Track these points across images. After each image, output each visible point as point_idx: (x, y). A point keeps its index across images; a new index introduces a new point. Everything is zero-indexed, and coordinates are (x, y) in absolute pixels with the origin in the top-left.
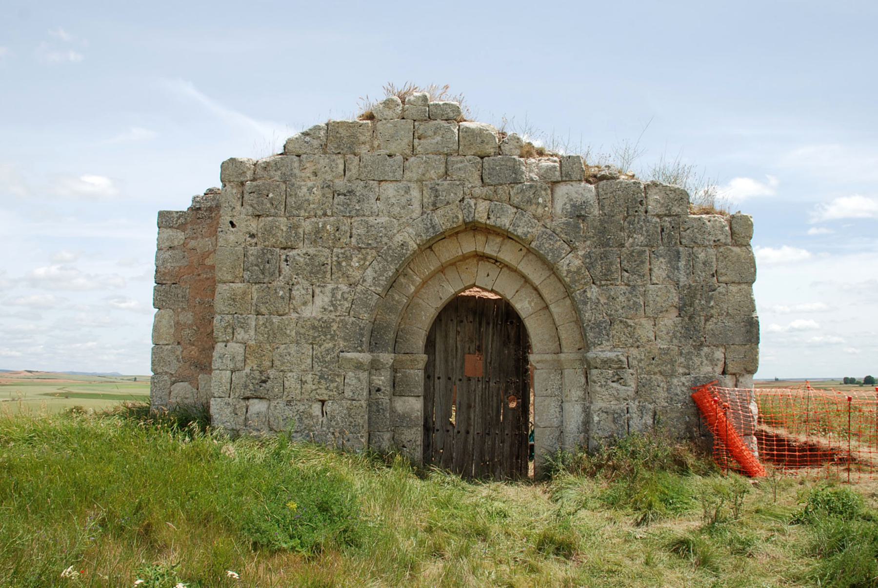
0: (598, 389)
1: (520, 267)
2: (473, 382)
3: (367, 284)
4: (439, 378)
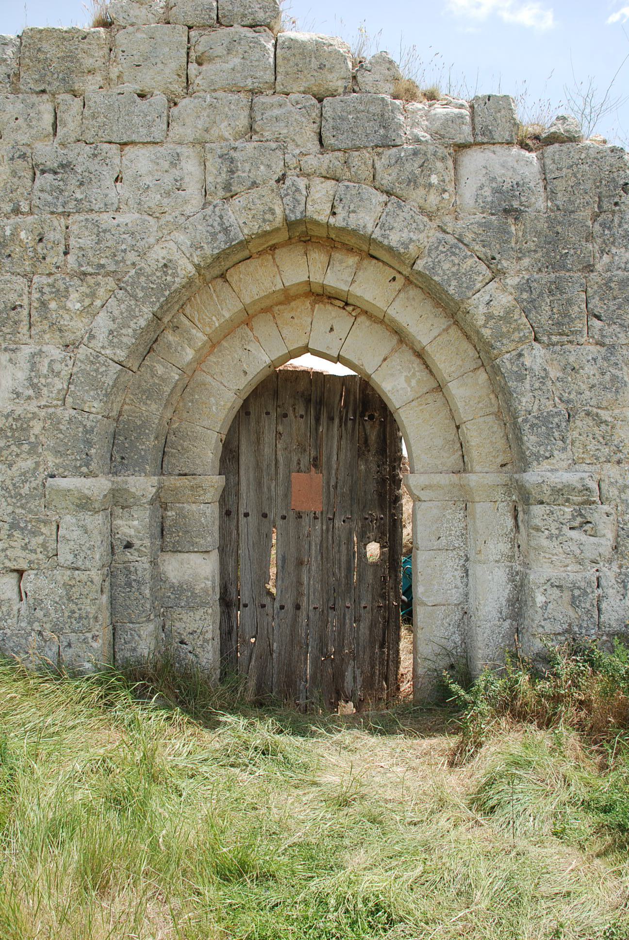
0: (545, 543)
1: (391, 312)
2: (306, 520)
3: (97, 344)
4: (246, 515)
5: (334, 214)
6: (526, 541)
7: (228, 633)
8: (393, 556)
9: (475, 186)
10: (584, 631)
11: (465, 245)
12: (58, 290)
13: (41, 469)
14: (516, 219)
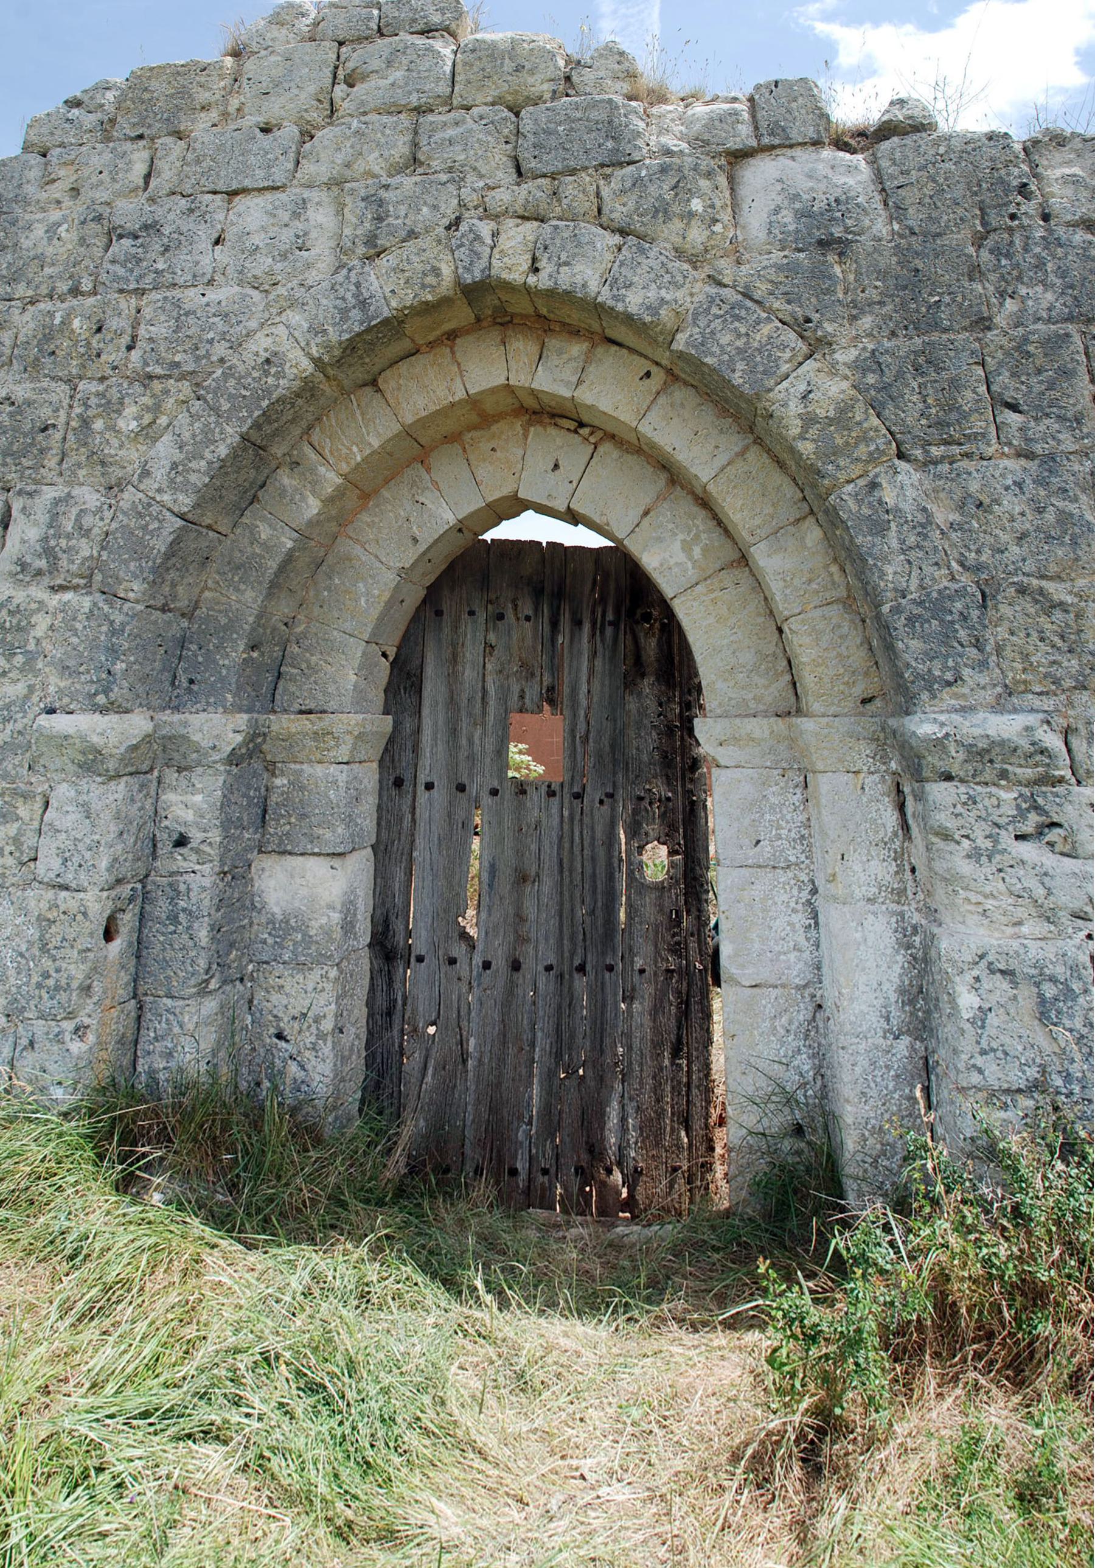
0: (965, 868)
1: (645, 428)
4: (429, 786)
5: (537, 270)
6: (924, 860)
7: (385, 1012)
8: (693, 870)
9: (766, 210)
10: (1077, 1089)
11: (757, 302)
12: (109, 402)
13: (35, 699)
14: (841, 254)
